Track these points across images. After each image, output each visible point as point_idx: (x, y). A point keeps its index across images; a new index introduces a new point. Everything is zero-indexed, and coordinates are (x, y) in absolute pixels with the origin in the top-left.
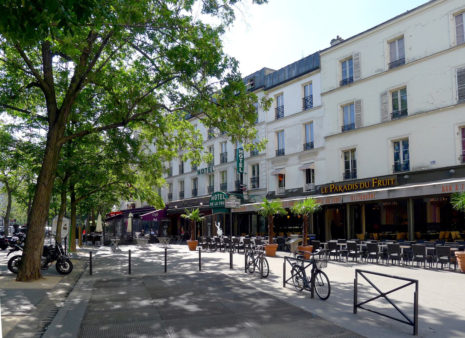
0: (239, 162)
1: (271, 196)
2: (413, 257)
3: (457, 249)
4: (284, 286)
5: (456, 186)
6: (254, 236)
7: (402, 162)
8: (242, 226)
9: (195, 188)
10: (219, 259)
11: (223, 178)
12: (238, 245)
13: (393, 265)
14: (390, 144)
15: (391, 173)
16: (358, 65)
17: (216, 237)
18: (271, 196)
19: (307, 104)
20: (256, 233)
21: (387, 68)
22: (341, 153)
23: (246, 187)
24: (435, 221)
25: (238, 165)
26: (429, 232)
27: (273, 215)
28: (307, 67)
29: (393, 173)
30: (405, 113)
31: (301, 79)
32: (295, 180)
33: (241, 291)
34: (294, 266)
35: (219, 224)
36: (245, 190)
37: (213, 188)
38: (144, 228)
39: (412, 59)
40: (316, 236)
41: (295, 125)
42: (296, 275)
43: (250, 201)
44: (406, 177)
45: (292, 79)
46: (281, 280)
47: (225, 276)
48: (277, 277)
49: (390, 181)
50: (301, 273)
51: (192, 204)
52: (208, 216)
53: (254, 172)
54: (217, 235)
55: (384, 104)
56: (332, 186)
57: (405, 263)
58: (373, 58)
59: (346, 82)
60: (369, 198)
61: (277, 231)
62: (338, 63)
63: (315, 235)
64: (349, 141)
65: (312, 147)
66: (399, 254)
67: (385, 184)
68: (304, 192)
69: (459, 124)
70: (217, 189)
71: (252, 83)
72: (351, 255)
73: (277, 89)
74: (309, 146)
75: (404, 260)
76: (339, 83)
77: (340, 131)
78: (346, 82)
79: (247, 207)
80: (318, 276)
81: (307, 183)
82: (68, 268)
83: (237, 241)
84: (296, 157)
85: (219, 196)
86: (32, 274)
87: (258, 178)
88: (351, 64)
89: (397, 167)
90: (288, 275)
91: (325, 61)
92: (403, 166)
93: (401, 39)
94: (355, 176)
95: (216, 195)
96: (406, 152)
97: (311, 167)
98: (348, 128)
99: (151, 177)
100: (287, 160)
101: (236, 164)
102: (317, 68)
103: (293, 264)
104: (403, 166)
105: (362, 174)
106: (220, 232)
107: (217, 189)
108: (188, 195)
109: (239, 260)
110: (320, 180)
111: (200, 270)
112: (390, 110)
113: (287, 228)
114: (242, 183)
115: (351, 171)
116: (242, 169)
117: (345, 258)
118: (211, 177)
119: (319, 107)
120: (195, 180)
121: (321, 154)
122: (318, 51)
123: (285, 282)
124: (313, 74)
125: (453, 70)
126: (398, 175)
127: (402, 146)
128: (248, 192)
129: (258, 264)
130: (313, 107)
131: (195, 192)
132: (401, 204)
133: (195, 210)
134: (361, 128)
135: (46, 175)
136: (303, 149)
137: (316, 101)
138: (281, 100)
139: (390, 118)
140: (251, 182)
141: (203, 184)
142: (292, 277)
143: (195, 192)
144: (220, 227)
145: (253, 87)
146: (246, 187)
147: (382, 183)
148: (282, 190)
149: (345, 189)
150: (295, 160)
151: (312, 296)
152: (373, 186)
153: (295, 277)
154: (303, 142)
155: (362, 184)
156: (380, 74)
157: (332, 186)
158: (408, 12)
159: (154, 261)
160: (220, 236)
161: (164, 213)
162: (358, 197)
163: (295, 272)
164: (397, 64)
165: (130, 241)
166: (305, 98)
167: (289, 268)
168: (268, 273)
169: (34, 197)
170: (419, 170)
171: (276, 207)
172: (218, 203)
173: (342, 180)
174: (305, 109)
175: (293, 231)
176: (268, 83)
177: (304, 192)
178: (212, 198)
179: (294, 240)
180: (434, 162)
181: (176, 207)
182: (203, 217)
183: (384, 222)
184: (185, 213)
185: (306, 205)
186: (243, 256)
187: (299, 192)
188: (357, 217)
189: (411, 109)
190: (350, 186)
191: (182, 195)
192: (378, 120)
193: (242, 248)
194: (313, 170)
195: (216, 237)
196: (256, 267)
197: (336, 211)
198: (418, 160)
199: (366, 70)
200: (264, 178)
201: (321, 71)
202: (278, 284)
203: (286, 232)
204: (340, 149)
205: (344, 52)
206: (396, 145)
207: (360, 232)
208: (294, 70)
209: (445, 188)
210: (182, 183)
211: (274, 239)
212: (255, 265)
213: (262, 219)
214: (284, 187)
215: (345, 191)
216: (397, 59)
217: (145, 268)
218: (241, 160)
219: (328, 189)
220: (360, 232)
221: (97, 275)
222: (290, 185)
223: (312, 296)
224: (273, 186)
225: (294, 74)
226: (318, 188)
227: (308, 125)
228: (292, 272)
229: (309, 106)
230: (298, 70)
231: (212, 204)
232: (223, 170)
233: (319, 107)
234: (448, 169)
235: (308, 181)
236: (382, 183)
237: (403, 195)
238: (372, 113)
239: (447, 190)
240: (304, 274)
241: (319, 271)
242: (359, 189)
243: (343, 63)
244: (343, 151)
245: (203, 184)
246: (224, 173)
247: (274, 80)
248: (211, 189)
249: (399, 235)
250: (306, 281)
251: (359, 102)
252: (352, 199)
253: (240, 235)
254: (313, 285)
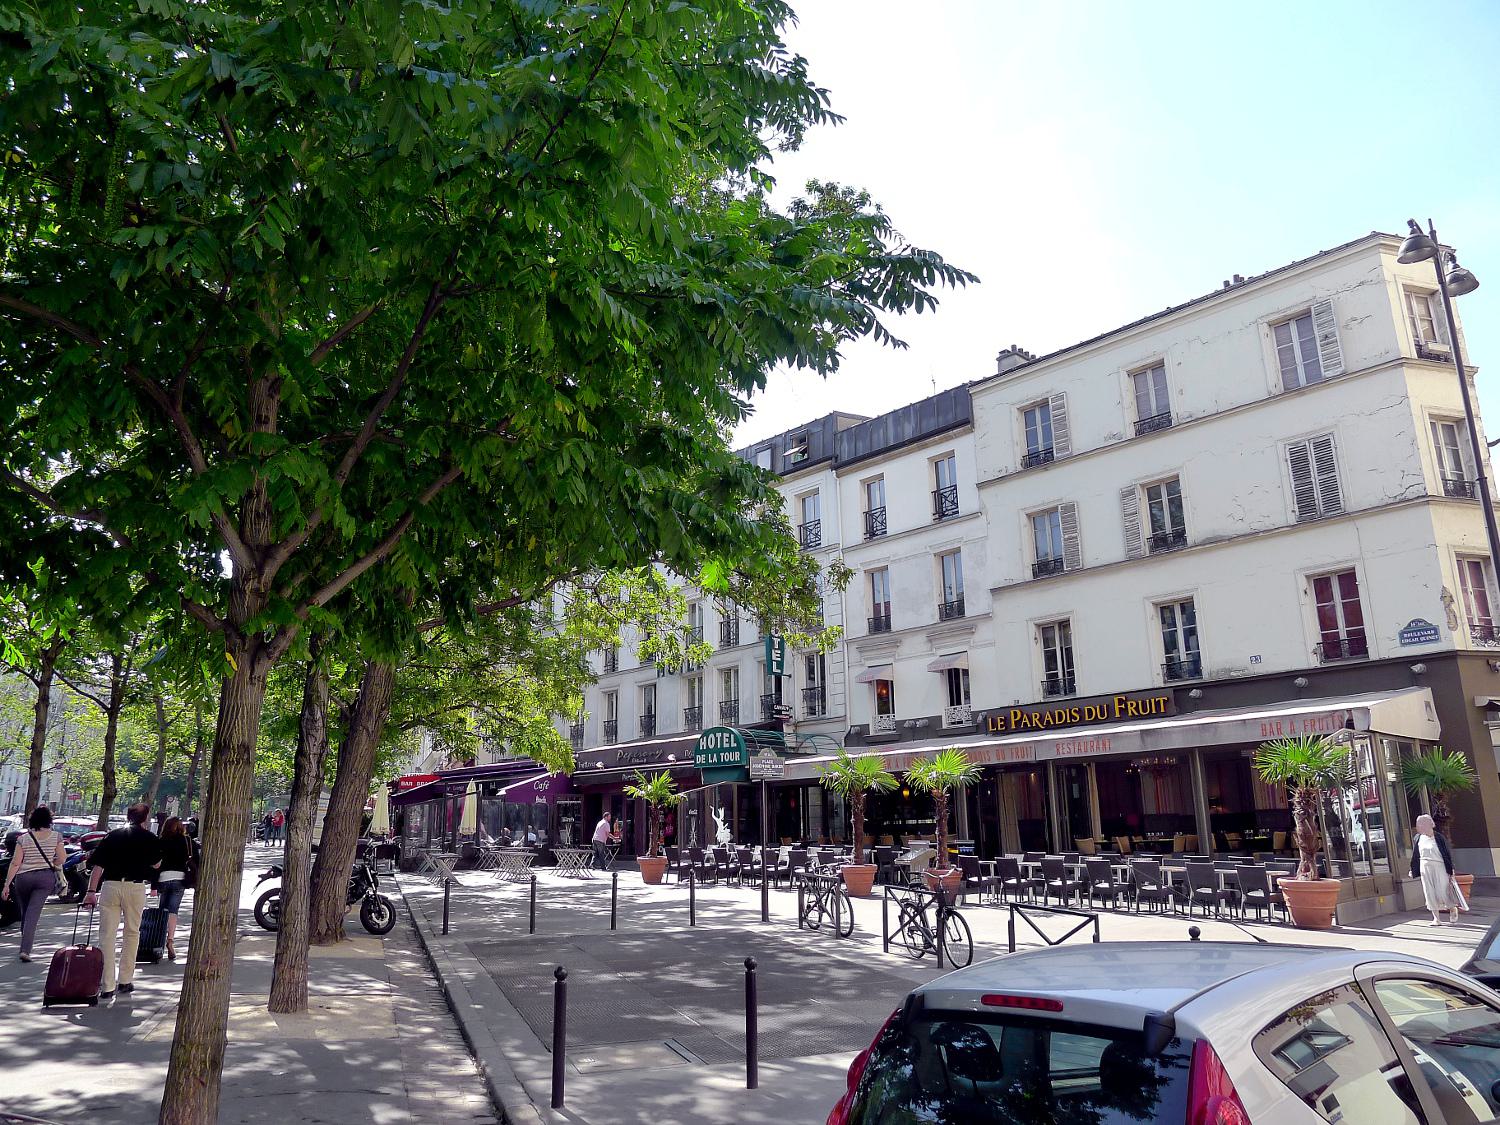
0: (770, 646)
1: (859, 737)
2: (1192, 894)
3: (1288, 873)
4: (886, 950)
5: (1292, 723)
6: (814, 844)
7: (1183, 658)
8: (778, 819)
9: (649, 709)
10: (730, 903)
11: (728, 690)
12: (776, 868)
13: (1151, 913)
14: (1152, 611)
15: (1159, 682)
16: (1062, 422)
17: (715, 847)
18: (859, 737)
19: (945, 506)
20: (820, 836)
21: (1131, 432)
22: (1033, 629)
23: (791, 713)
24: (1274, 803)
25: (769, 654)
26: (1250, 835)
27: (864, 791)
28: (941, 419)
29: (1165, 682)
30: (1180, 536)
31: (925, 447)
32: (920, 695)
33: (799, 960)
34: (905, 904)
35: (722, 812)
36: (787, 721)
37: (700, 714)
38: (505, 821)
39: (1187, 415)
40: (974, 845)
41: (915, 556)
42: (909, 923)
43: (801, 751)
44: (1194, 693)
45: (903, 444)
46: (880, 940)
47: (750, 935)
48: (874, 936)
49: (1157, 704)
50: (918, 919)
51: (650, 757)
52: (703, 790)
53: (811, 671)
54: (716, 842)
55: (1130, 516)
56: (1015, 713)
57: (1179, 908)
58: (1098, 407)
59: (1038, 460)
60: (1098, 748)
61: (875, 831)
62: (1016, 413)
63: (973, 842)
64: (1052, 601)
65: (961, 611)
66: (1214, 891)
67: (1145, 710)
68: (944, 727)
69: (1308, 568)
70: (712, 718)
71: (803, 447)
72: (1055, 892)
73: (867, 466)
74: (953, 610)
75: (1177, 901)
76: (1019, 460)
77: (1029, 575)
78: (1038, 460)
79: (793, 769)
80: (950, 922)
81: (952, 704)
82: (386, 920)
83: (772, 858)
84: (922, 638)
85: (722, 738)
86: (329, 929)
87: (823, 688)
88: (1045, 418)
89: (1172, 669)
90: (894, 925)
91: (982, 406)
92: (1185, 667)
93: (1158, 366)
94: (1073, 690)
95: (712, 736)
96: (1191, 633)
97: (959, 664)
98: (1047, 569)
99: (552, 695)
100: (896, 644)
101: (762, 650)
102: (966, 422)
103: (903, 900)
104: (1185, 667)
105: (1089, 683)
106: (723, 834)
107: (712, 718)
108: (630, 733)
109: (785, 904)
110: (984, 697)
111: (693, 924)
112: (1146, 530)
113: (904, 822)
114: (779, 703)
115: (1060, 676)
116: (780, 665)
117: (1041, 899)
118: (695, 682)
119: (974, 515)
120: (650, 689)
121: (984, 632)
122: (967, 381)
123: (887, 941)
124: (956, 436)
125: (1280, 445)
126: (1176, 690)
127: (1178, 618)
128: (796, 725)
129: (828, 907)
130: (960, 514)
131: (649, 723)
132: (1173, 765)
133: (659, 776)
134: (1080, 572)
135: (371, 710)
136: (937, 617)
137: (967, 501)
138: (878, 492)
139: (1146, 550)
140: (805, 698)
141: (672, 700)
142: (901, 929)
143: (649, 723)
144: (725, 822)
145: (806, 456)
146: (791, 713)
147: (1137, 708)
148: (887, 722)
149: (1048, 722)
150: (918, 643)
151: (940, 965)
152: (1118, 715)
153: (906, 928)
154: (937, 601)
155: (1090, 711)
156: (1115, 445)
157: (1015, 713)
158: (1170, 311)
159: (569, 906)
160: (724, 845)
161: (564, 784)
162: (1071, 747)
163: (907, 918)
164: (1154, 424)
165: (472, 860)
166: (938, 490)
167: (894, 910)
168: (852, 928)
169: (698, 817)
170: (1226, 677)
171: (870, 773)
172: (719, 758)
173: (1039, 698)
174: (940, 518)
175: (919, 832)
176: (845, 451)
177: (944, 727)
178: (703, 744)
179: (915, 854)
180: (1257, 659)
181: (599, 765)
182: (681, 794)
183: (1149, 808)
184: (635, 783)
185: (944, 765)
186: (794, 896)
187: (930, 729)
188: (1076, 795)
189: (1192, 534)
190: (1060, 714)
191: (611, 730)
192: (1118, 553)
193: (785, 876)
194: (966, 672)
195: (715, 847)
196: (825, 915)
197: (1028, 777)
198: (1219, 655)
199: (1082, 436)
200: (840, 688)
201: (976, 430)
202: (876, 947)
203: (900, 835)
204: (1031, 620)
205: (1031, 388)
206: (1167, 614)
207: (1086, 832)
208: (910, 422)
209: (1268, 727)
210: (612, 696)
211: (866, 851)
212: (822, 910)
213: (838, 798)
214: (891, 715)
215: (1049, 727)
216: (1154, 413)
217: (556, 920)
218: (777, 641)
219: (1006, 721)
220: (1086, 832)
221: (456, 935)
222: (906, 708)
223: (940, 965)
224: (863, 711)
225: (909, 431)
226: (980, 718)
227: (948, 557)
228: (901, 918)
229: (950, 512)
230: (919, 424)
231: (701, 759)
232: (727, 666)
233: (974, 515)
234: (1290, 676)
235: (955, 698)
236: (1137, 708)
237: (1177, 743)
238: (1102, 535)
239: (1272, 732)
240: (924, 920)
241: (951, 913)
242: (1082, 723)
243: (1028, 413)
244: (1038, 626)
245: (672, 700)
246: (729, 674)
247: (860, 445)
248: (693, 715)
249: (1178, 840)
250: (928, 934)
251: (1070, 509)
252: (1058, 753)
253: (776, 840)
254: (942, 939)
